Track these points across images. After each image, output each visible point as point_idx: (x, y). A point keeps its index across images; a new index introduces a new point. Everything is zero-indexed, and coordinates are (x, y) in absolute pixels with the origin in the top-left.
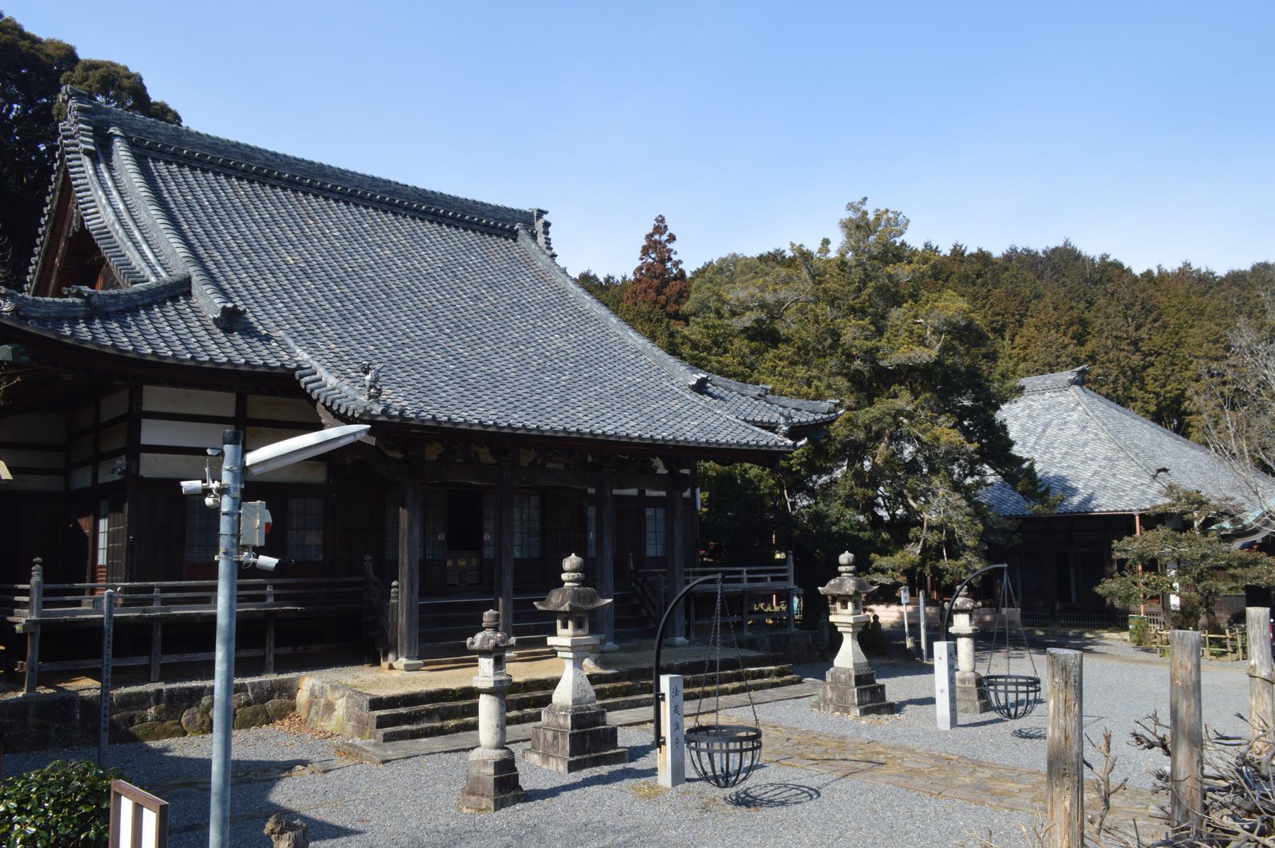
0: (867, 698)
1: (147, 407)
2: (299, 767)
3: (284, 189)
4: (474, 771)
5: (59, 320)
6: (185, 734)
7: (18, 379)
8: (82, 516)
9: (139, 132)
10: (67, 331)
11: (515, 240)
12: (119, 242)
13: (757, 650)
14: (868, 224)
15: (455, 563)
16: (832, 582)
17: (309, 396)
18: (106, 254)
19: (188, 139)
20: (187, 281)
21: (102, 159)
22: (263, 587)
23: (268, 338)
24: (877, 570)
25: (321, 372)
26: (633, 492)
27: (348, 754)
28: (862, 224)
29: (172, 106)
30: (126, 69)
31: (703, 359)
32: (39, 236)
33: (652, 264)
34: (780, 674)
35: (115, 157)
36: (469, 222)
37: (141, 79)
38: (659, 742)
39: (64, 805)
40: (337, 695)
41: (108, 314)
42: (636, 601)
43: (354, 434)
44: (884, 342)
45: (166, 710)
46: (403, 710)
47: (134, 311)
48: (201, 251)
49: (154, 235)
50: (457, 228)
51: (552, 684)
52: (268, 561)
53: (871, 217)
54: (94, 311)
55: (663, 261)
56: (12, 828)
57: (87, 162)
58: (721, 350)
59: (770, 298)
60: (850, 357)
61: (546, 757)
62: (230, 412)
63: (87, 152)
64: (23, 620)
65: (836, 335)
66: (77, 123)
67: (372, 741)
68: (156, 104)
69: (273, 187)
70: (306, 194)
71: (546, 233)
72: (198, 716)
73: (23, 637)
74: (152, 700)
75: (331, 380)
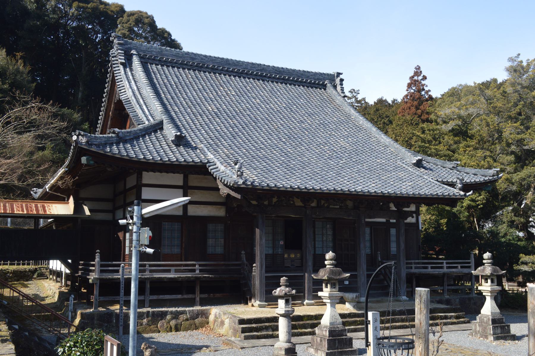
0: (499, 331)
1: (145, 181)
2: (205, 348)
3: (210, 73)
4: (276, 352)
5: (105, 145)
6: (159, 332)
7: (77, 178)
8: (119, 232)
9: (144, 51)
10: (108, 149)
11: (325, 89)
12: (134, 105)
13: (452, 305)
14: (523, 68)
15: (289, 255)
16: (479, 268)
17: (212, 175)
18: (129, 111)
19: (165, 53)
20: (161, 123)
21: (128, 66)
22: (194, 265)
23: (196, 148)
24: (523, 263)
25: (218, 164)
26: (383, 220)
27: (227, 344)
28: (519, 68)
29: (168, 30)
30: (146, 13)
31: (427, 147)
32: (103, 102)
33: (413, 93)
34: (457, 317)
35: (133, 64)
36: (301, 82)
37: (153, 17)
38: (368, 345)
39: (90, 345)
40: (226, 317)
41: (126, 140)
42: (382, 277)
43: (184, 201)
44: (527, 136)
45: (151, 320)
46: (254, 325)
47: (137, 138)
48: (169, 107)
49: (148, 101)
50: (295, 85)
51: (322, 316)
52: (150, 251)
53: (525, 64)
54: (121, 140)
55: (419, 91)
56: (72, 352)
57: (121, 68)
58: (437, 142)
59: (463, 113)
60: (509, 145)
61: (317, 350)
62: (181, 183)
63: (122, 64)
64: (92, 278)
65: (500, 132)
66: (117, 50)
67: (239, 339)
68: (160, 29)
69: (205, 72)
70: (220, 74)
71: (341, 84)
72: (165, 324)
73: (93, 285)
74: (145, 316)
75: (222, 168)
